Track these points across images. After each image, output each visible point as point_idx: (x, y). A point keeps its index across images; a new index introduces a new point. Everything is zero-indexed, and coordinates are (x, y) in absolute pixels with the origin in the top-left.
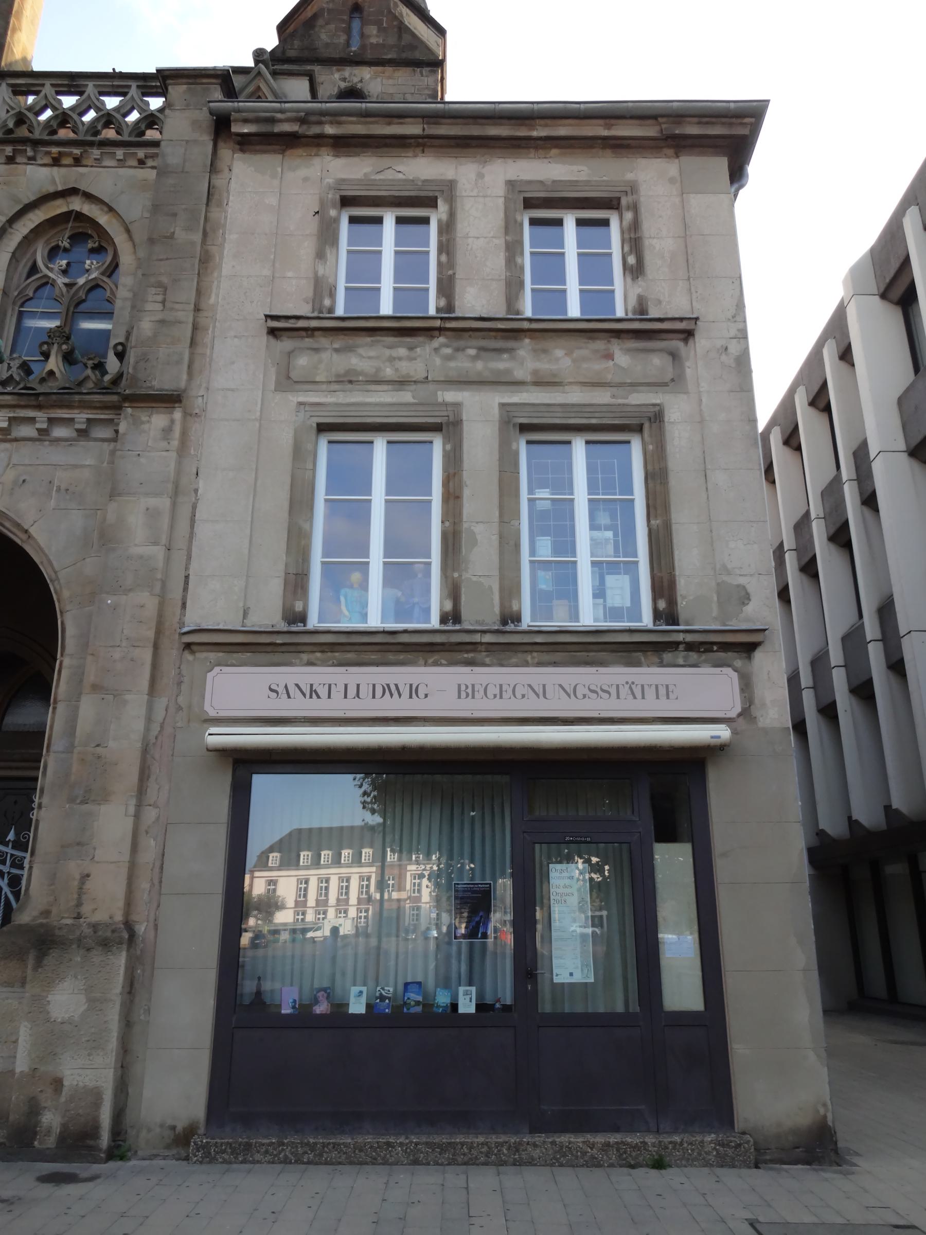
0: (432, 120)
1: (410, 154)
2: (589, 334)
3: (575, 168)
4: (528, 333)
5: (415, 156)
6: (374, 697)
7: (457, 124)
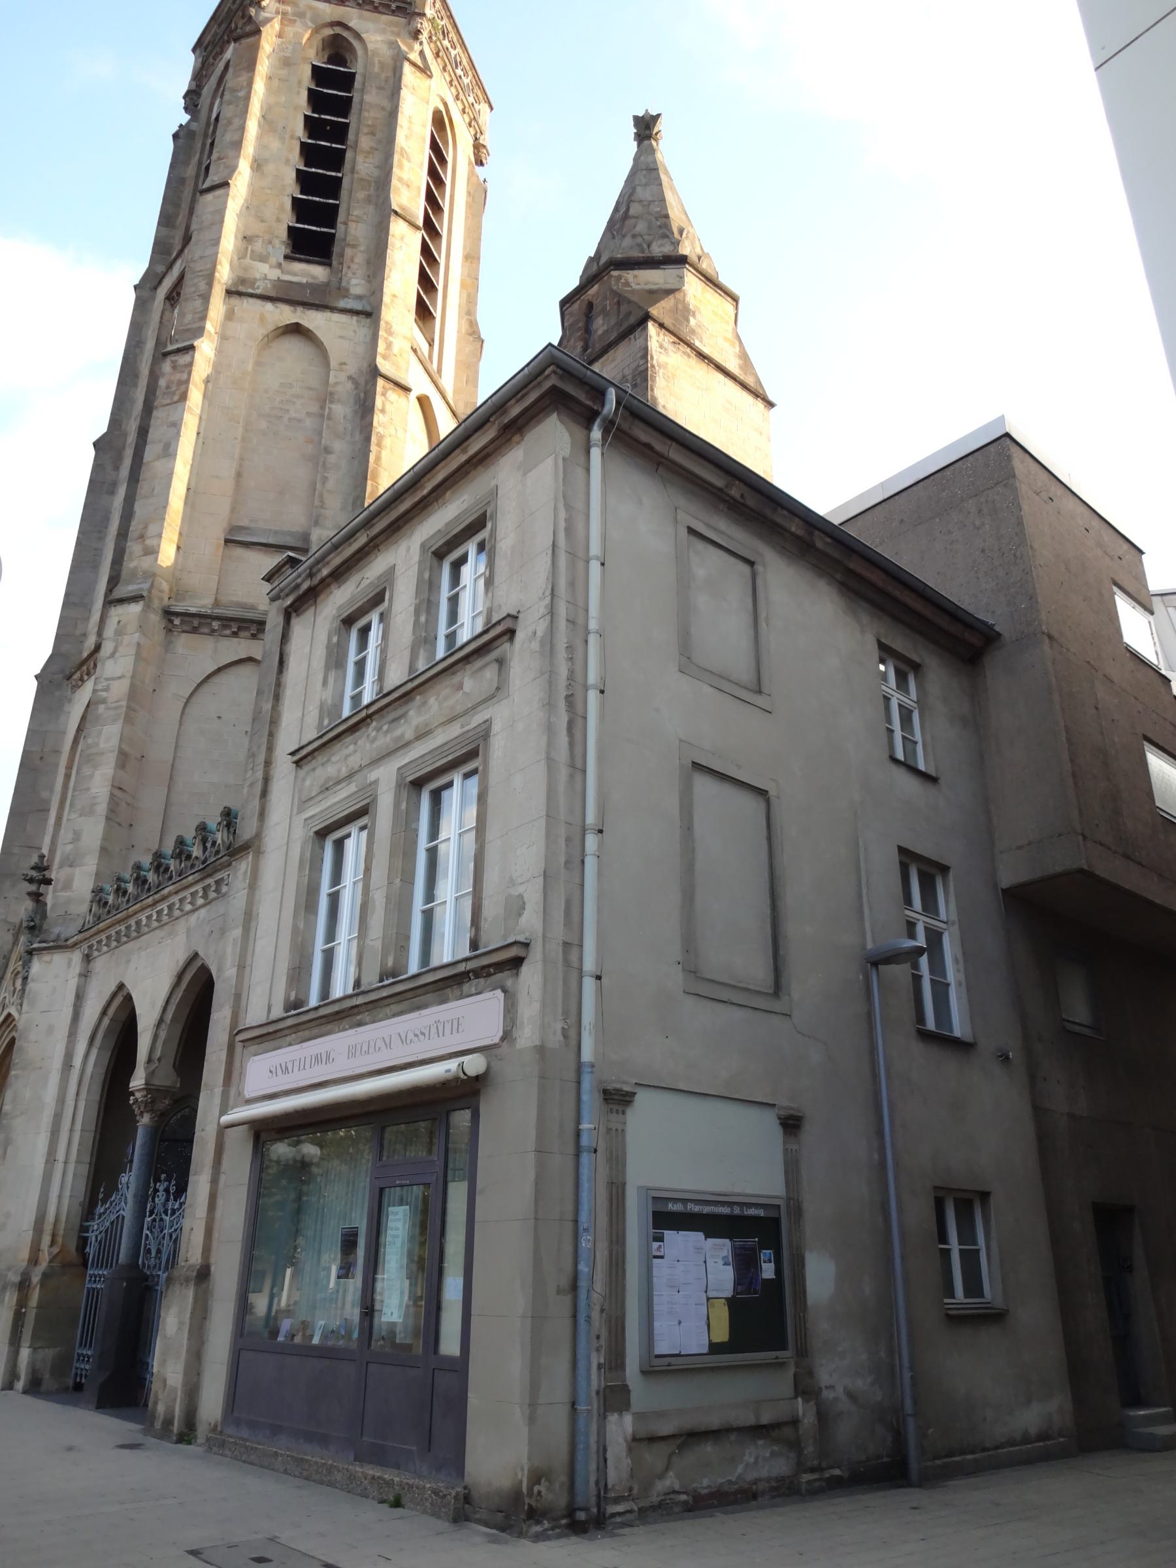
0: (368, 526)
1: (374, 557)
2: (451, 670)
3: (466, 497)
4: (415, 692)
5: (376, 557)
6: (439, 1036)
7: (383, 517)
